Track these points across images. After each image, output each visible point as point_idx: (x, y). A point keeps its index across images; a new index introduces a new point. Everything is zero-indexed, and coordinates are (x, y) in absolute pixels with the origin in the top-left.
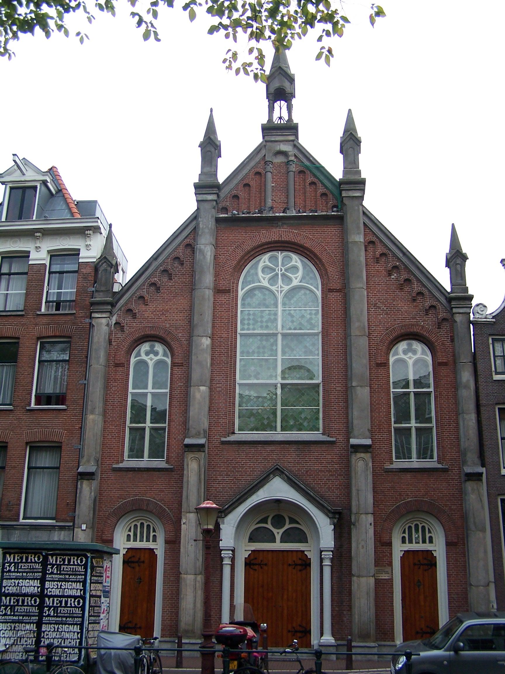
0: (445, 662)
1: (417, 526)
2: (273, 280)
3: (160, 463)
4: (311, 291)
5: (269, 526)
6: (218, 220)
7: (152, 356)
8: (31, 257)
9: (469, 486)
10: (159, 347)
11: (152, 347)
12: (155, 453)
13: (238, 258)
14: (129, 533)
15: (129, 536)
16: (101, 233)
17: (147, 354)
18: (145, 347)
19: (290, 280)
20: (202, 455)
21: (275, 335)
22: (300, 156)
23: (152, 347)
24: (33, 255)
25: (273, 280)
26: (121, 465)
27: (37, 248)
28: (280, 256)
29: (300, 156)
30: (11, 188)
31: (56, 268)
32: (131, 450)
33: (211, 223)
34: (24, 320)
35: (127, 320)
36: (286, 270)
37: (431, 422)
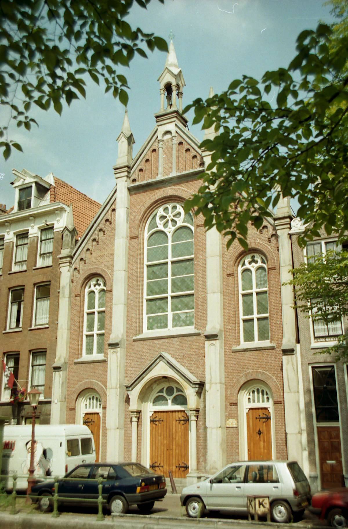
0: (154, 479)
1: (258, 390)
2: (165, 225)
3: (266, 343)
4: (189, 228)
5: (164, 394)
6: (129, 189)
7: (253, 264)
8: (6, 238)
9: (285, 359)
10: (258, 258)
11: (253, 257)
12: (263, 336)
13: (142, 213)
14: (250, 397)
15: (249, 399)
16: (66, 211)
17: (250, 263)
18: (93, 282)
19: (176, 222)
20: (217, 343)
21: (166, 263)
22: (179, 131)
23: (253, 257)
24: (6, 237)
25: (165, 225)
26: (80, 360)
27: (32, 227)
28: (170, 206)
29: (179, 131)
30: (20, 190)
31: (20, 243)
32: (87, 349)
33: (125, 192)
34: (26, 273)
35: (81, 266)
36: (174, 216)
37: (175, 326)
